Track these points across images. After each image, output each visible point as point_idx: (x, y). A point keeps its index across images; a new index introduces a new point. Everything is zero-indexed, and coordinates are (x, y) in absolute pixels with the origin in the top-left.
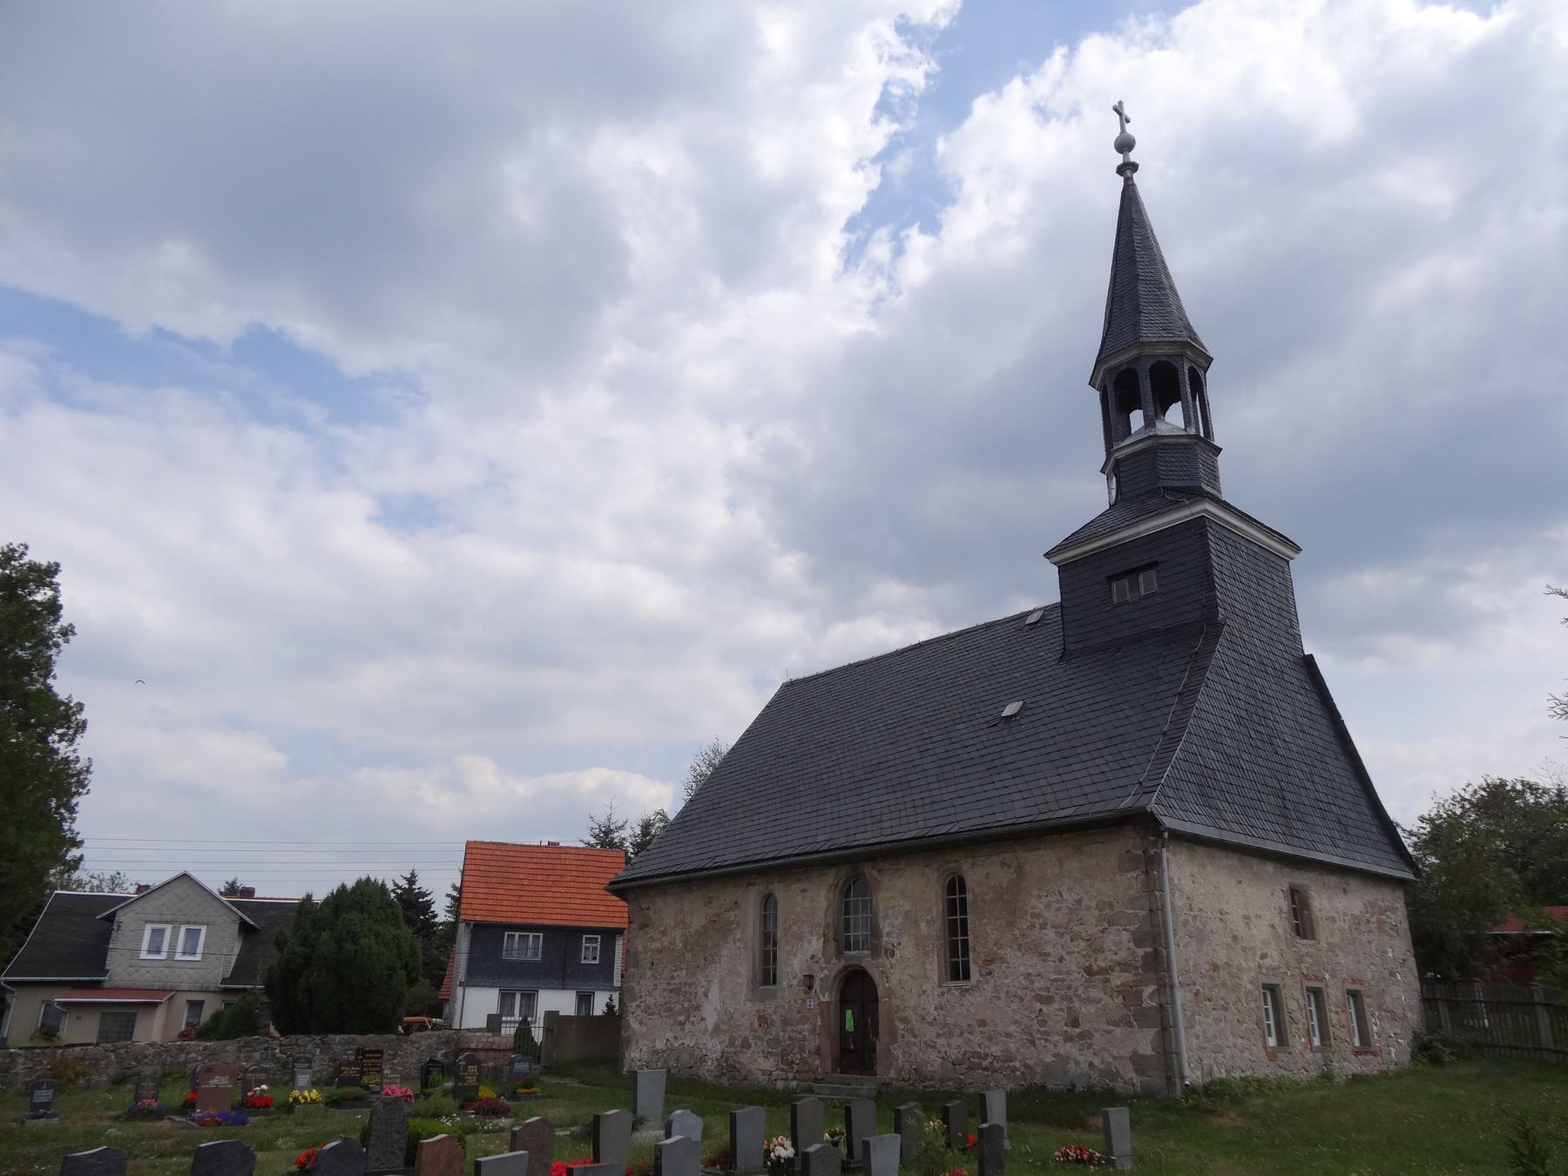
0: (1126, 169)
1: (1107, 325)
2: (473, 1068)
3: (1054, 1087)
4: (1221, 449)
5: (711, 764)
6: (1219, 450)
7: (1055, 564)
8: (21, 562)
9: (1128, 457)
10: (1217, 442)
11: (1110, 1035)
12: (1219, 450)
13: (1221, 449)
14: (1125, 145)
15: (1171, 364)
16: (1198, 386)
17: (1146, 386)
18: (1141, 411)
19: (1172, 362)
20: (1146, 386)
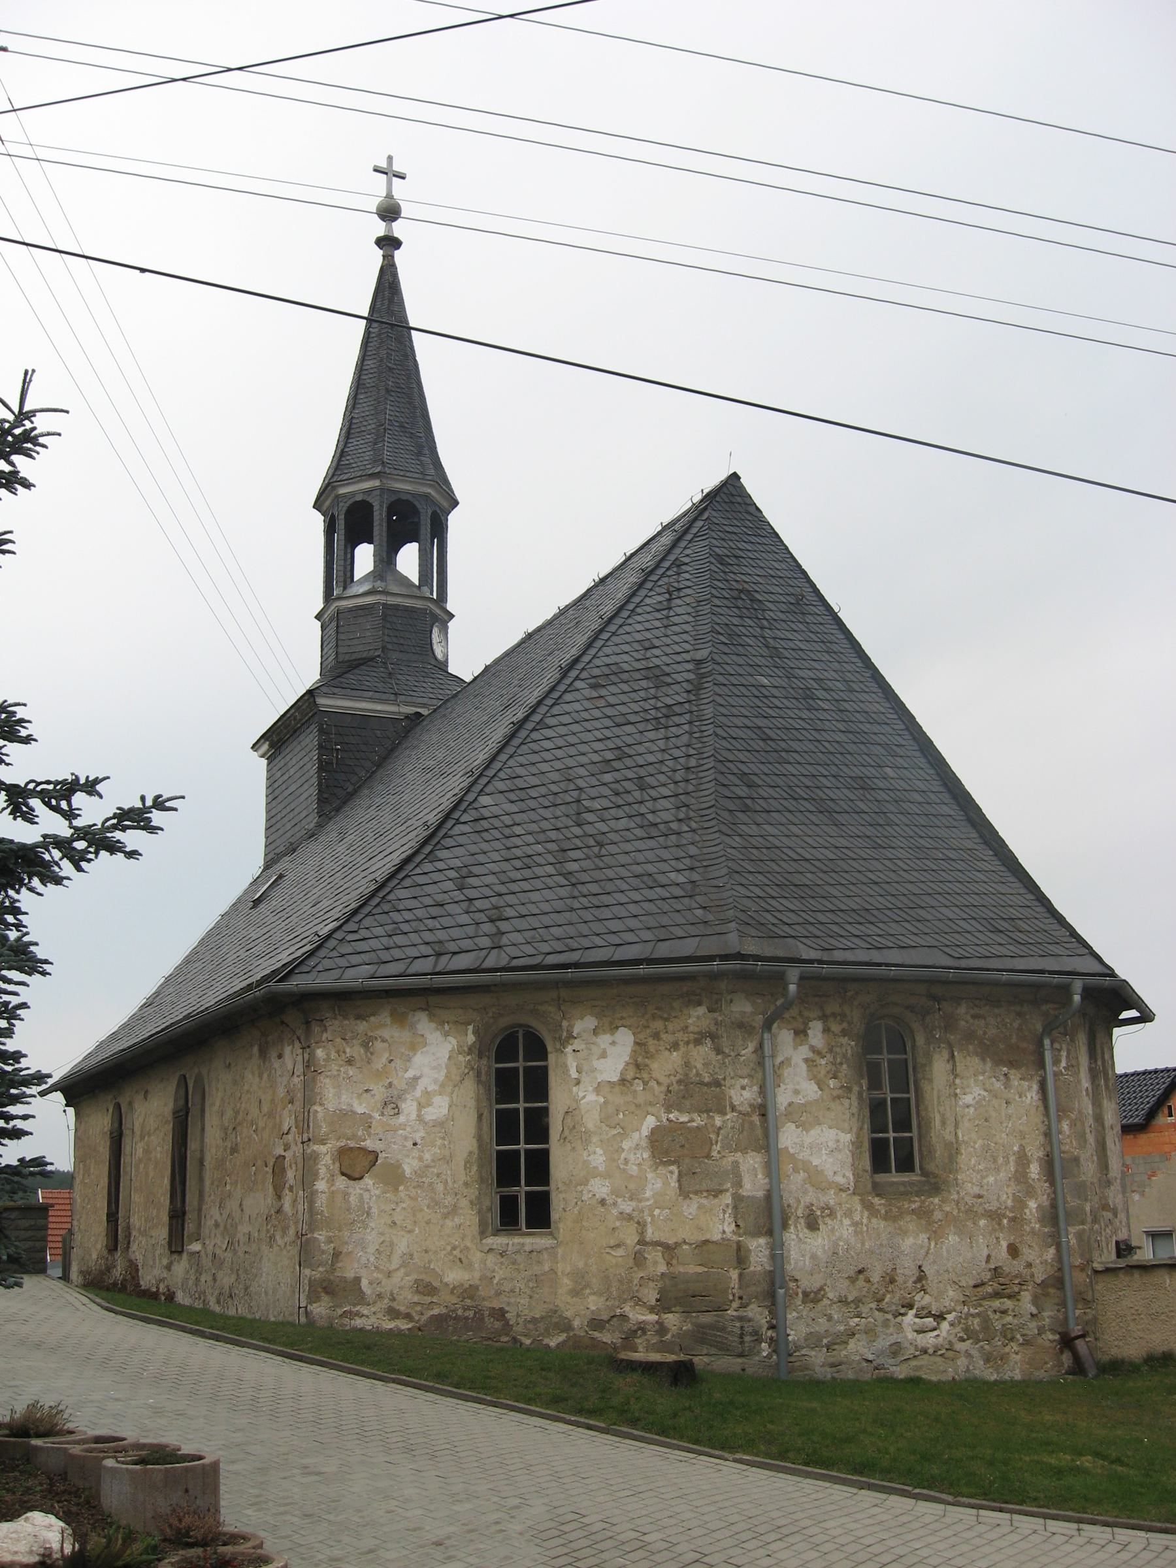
0: (388, 243)
1: (351, 402)
2: (857, 1218)
3: (760, 1176)
4: (453, 616)
5: (426, 1288)
6: (452, 616)
7: (262, 756)
8: (17, 1066)
9: (351, 610)
10: (450, 606)
11: (442, 1547)
12: (452, 616)
13: (453, 616)
14: (389, 212)
15: (414, 506)
16: (439, 530)
17: (379, 527)
18: (371, 547)
19: (416, 503)
20: (379, 527)
